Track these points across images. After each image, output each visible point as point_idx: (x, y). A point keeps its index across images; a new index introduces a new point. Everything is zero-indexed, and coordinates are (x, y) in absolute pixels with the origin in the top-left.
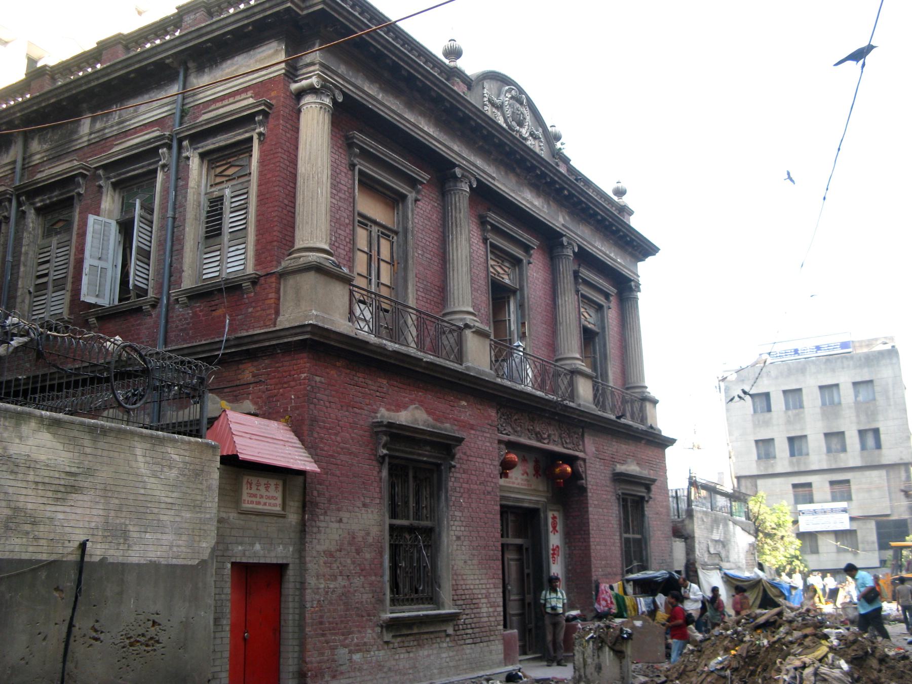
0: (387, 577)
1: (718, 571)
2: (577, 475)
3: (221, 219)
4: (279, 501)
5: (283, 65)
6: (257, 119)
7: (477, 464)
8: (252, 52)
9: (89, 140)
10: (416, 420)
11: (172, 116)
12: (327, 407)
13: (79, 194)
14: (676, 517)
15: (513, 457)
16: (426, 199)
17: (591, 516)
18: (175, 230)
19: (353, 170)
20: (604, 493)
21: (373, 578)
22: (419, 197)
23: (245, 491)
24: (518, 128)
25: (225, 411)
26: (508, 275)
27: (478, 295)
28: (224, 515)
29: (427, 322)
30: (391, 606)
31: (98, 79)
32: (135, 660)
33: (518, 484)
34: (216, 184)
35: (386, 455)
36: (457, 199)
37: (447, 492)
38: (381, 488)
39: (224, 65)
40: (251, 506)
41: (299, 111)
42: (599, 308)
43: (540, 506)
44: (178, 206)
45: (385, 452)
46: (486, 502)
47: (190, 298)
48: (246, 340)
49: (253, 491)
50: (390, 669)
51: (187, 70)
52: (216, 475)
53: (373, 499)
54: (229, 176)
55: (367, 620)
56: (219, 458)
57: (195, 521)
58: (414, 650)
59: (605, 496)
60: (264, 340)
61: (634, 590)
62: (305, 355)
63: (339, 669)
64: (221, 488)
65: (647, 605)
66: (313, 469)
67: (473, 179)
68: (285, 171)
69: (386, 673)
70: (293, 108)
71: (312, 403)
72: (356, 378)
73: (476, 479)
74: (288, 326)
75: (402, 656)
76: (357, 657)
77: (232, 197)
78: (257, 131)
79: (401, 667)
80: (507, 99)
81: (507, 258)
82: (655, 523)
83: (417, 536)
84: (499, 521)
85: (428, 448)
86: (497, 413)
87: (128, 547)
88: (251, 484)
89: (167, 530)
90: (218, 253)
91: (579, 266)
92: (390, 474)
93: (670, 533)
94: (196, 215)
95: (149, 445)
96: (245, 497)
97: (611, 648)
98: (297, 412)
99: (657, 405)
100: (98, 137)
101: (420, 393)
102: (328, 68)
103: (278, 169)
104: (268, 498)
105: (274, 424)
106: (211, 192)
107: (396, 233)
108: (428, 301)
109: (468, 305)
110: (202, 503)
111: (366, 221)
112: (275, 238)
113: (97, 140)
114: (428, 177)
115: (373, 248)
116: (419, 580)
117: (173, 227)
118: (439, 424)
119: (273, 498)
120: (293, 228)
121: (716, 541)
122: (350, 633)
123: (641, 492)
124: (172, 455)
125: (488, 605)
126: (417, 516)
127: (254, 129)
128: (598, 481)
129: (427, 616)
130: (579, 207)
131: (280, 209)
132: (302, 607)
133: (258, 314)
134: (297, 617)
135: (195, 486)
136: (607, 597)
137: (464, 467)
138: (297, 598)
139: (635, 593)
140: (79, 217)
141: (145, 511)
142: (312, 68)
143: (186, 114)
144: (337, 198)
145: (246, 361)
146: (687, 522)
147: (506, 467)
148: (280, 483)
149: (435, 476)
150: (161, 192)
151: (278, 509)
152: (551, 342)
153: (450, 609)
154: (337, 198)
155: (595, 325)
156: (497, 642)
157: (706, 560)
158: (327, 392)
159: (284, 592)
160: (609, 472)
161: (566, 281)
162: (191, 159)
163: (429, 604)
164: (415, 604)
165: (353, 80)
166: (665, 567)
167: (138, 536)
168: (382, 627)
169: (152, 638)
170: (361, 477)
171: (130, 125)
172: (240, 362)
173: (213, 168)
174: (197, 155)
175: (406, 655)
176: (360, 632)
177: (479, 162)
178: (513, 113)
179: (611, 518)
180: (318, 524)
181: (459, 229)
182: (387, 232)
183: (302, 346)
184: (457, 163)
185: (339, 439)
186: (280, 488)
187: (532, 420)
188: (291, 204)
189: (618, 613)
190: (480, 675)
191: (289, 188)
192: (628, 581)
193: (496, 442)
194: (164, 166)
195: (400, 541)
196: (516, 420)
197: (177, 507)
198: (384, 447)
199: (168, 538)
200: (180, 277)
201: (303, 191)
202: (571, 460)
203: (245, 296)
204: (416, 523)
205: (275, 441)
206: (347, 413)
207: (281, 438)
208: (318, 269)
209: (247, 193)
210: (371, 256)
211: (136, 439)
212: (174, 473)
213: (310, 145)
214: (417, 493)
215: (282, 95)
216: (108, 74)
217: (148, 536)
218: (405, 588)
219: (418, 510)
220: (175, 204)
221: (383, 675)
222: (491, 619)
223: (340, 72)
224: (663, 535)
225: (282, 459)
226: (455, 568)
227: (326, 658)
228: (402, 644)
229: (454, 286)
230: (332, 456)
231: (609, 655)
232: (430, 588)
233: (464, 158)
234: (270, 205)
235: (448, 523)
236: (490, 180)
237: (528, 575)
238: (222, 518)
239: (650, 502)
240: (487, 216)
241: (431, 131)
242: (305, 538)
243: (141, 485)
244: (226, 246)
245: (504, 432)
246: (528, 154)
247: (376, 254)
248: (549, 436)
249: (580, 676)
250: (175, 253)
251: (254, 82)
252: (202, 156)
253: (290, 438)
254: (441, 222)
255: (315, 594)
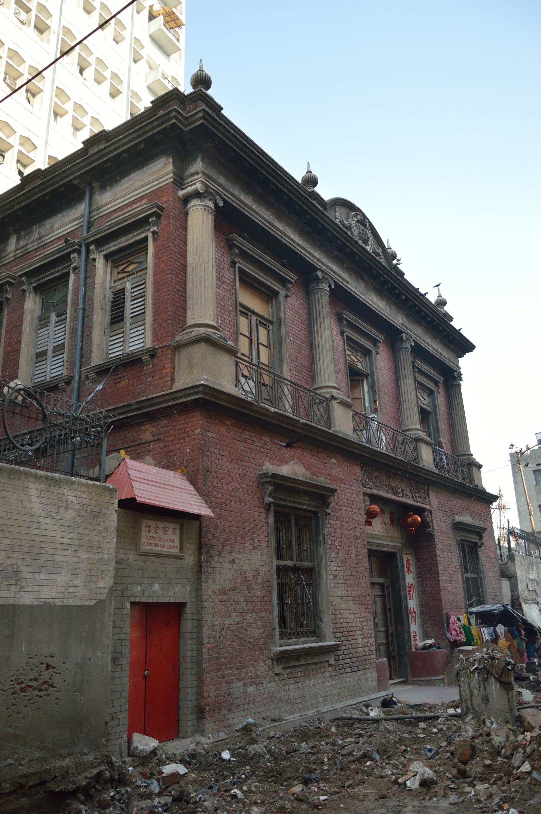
0: (276, 613)
1: (536, 605)
2: (425, 524)
3: (123, 307)
4: (177, 544)
5: (171, 175)
6: (150, 220)
7: (347, 513)
8: (145, 168)
9: (14, 256)
10: (296, 473)
11: (81, 228)
12: (219, 460)
13: (7, 299)
14: (500, 561)
15: (375, 508)
16: (293, 296)
17: (439, 559)
18: (85, 319)
19: (234, 267)
20: (447, 539)
21: (264, 613)
22: (289, 294)
23: (144, 534)
24: (364, 245)
25: (124, 459)
26: (361, 363)
27: (339, 376)
28: (123, 556)
29: (301, 393)
30: (280, 639)
31: (19, 203)
32: (26, 706)
33: (379, 532)
34: (119, 280)
35: (271, 503)
36: (319, 297)
37: (324, 536)
38: (268, 532)
39: (122, 182)
40: (150, 548)
41: (187, 214)
42: (431, 393)
43: (397, 551)
44: (87, 300)
45: (271, 500)
46: (356, 545)
47: (98, 374)
48: (146, 404)
49: (152, 534)
50: (281, 700)
51: (92, 189)
52: (114, 517)
53: (261, 542)
54: (129, 272)
55: (259, 654)
56: (116, 501)
57: (92, 562)
58: (301, 680)
59: (448, 542)
60: (162, 402)
61: (476, 621)
62: (198, 413)
63: (234, 702)
64: (119, 531)
65: (489, 634)
66: (208, 513)
67: (331, 282)
68: (177, 262)
69: (277, 703)
70: (181, 211)
71: (205, 456)
72: (243, 436)
73: (347, 525)
74: (181, 388)
75: (291, 686)
76: (251, 689)
77: (132, 288)
78: (151, 230)
79: (291, 697)
80: (354, 222)
81: (360, 349)
82: (487, 564)
83: (300, 575)
84: (367, 562)
85: (307, 498)
86: (361, 470)
87: (20, 588)
88: (150, 527)
89: (63, 571)
90: (121, 335)
91: (415, 358)
92: (276, 521)
93: (498, 573)
94: (102, 306)
95: (44, 486)
96: (144, 539)
97: (497, 679)
98: (192, 464)
99: (481, 469)
100: (22, 252)
101: (298, 451)
102: (210, 177)
103: (170, 259)
104: (166, 540)
105: (171, 474)
106: (115, 286)
107: (272, 323)
108: (300, 379)
109: (332, 381)
110: (99, 544)
111: (246, 311)
112: (170, 317)
113: (22, 254)
114: (295, 277)
115: (253, 333)
116: (303, 614)
117: (83, 317)
118: (315, 478)
119: (171, 540)
120: (185, 310)
121: (532, 580)
122: (244, 667)
123: (475, 539)
124: (69, 497)
125: (363, 637)
126: (300, 558)
127: (149, 230)
128: (442, 529)
129: (312, 648)
130: (413, 310)
131: (173, 293)
132: (200, 643)
133: (156, 382)
134: (195, 653)
135: (92, 528)
136: (456, 628)
137: (337, 514)
138: (194, 635)
139: (477, 624)
140: (7, 318)
141: (39, 551)
142: (196, 177)
143: (93, 225)
144: (222, 288)
145: (147, 423)
146: (509, 564)
147: (370, 515)
148: (178, 527)
149: (313, 522)
150: (73, 290)
151: (175, 551)
152: (397, 417)
153: (331, 641)
154: (222, 288)
155: (428, 406)
156: (371, 670)
157: (526, 596)
158: (218, 446)
159: (183, 629)
160: (450, 522)
161: (406, 368)
162: (97, 260)
163: (312, 636)
164: (300, 638)
165: (231, 190)
166: (497, 602)
167: (32, 577)
168: (273, 659)
169: (45, 682)
170: (250, 522)
171: (47, 239)
172: (141, 424)
173: (116, 267)
174: (102, 257)
175: (295, 686)
176: (253, 665)
177: (335, 268)
178: (359, 233)
179: (454, 560)
180: (213, 565)
181: (322, 320)
182: (263, 322)
183: (196, 405)
184: (318, 267)
185: (230, 488)
186: (178, 532)
187: (389, 477)
188: (182, 290)
189: (466, 641)
190: (359, 701)
191: (180, 276)
192: (471, 613)
193: (362, 494)
194: (75, 268)
195: (286, 580)
196: (376, 476)
197: (73, 548)
198: (270, 495)
199: (64, 578)
200: (90, 358)
201: (193, 278)
202: (420, 511)
203: (145, 368)
204: (298, 564)
205: (172, 488)
206: (237, 466)
207: (178, 486)
208: (208, 340)
209: (144, 283)
210: (251, 340)
211: (30, 479)
212: (71, 514)
213: (197, 240)
214: (299, 537)
215: (172, 199)
216: (28, 198)
217: (42, 576)
218: (291, 623)
219: (300, 552)
220: (84, 298)
221: (275, 706)
222: (366, 649)
223: (220, 181)
224: (494, 575)
225: (178, 504)
226: (334, 603)
227: (222, 692)
228: (290, 676)
229: (320, 366)
230: (224, 503)
231: (496, 686)
232: (313, 622)
233: (323, 264)
234: (165, 290)
235: (326, 564)
236: (345, 283)
237: (390, 609)
238: (122, 559)
239: (482, 548)
240: (343, 314)
241: (296, 239)
242: (201, 578)
243: (35, 525)
244: (128, 329)
245: (367, 486)
246: (374, 263)
247: (256, 339)
248: (403, 491)
249: (468, 708)
250: (85, 338)
251: (148, 192)
252: (107, 257)
253: (186, 486)
254: (307, 316)
255: (211, 631)
